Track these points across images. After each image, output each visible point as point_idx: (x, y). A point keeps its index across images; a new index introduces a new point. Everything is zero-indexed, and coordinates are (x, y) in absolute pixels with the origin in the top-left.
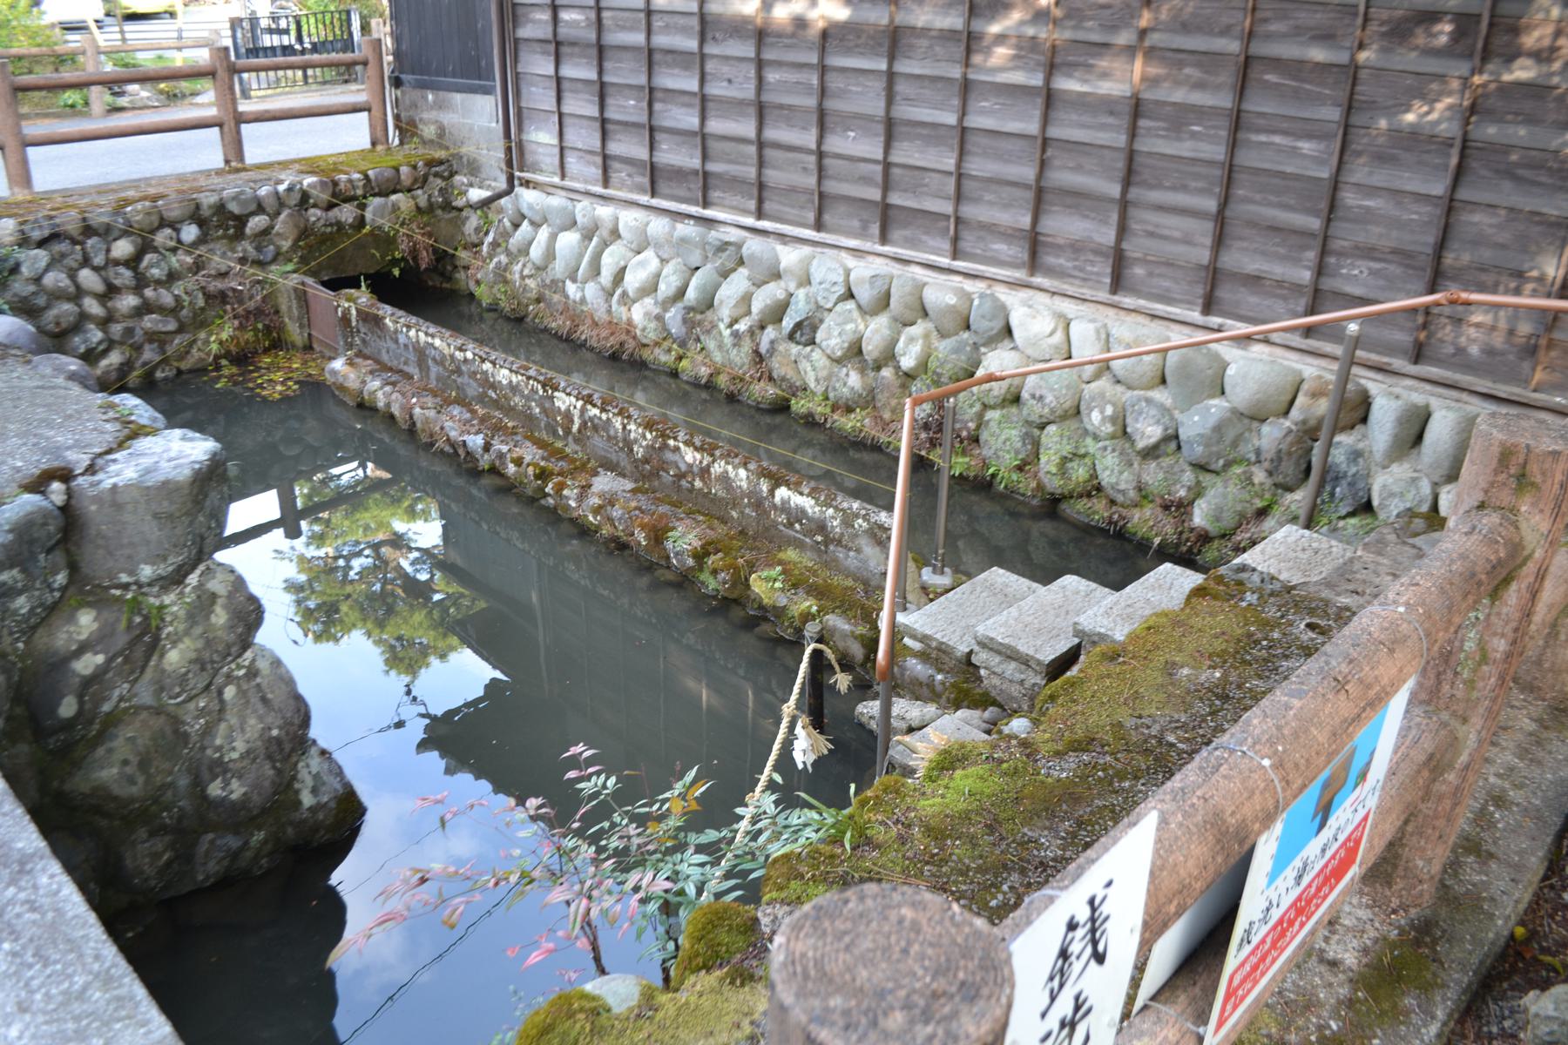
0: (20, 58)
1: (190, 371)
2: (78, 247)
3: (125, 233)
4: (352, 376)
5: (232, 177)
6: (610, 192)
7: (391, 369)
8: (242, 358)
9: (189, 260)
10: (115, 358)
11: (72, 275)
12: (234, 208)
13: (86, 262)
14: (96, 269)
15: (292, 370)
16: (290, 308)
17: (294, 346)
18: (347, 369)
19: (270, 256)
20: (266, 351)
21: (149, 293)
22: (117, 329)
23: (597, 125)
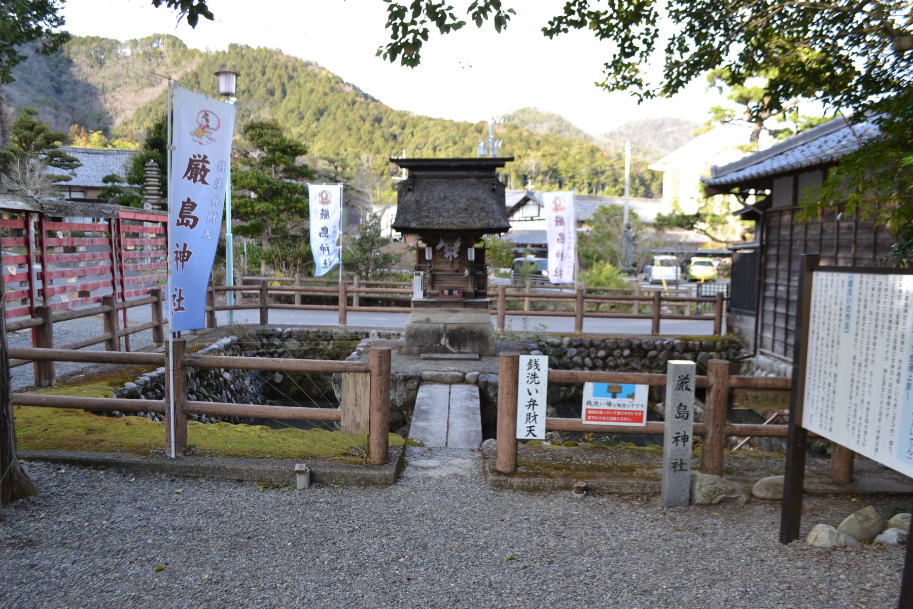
6: (786, 358)
11: (583, 359)
12: (645, 346)
13: (588, 355)
14: (591, 359)
23: (784, 331)
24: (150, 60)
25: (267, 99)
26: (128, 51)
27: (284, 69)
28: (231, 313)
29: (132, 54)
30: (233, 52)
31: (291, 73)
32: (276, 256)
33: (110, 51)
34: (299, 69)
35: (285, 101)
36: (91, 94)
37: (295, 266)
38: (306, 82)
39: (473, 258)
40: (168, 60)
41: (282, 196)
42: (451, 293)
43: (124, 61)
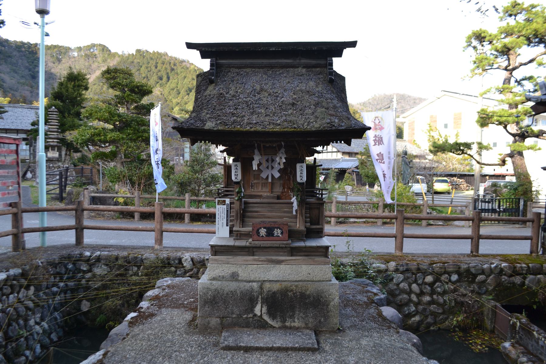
0: (403, 205)
1: (443, 330)
2: (414, 276)
3: (431, 274)
4: (513, 352)
5: (473, 258)
7: (532, 354)
8: (464, 329)
9: (452, 287)
10: (417, 318)
11: (410, 285)
12: (473, 270)
13: (415, 281)
14: (418, 285)
15: (484, 339)
16: (488, 314)
17: (487, 329)
18: (510, 348)
19: (483, 291)
20: (475, 329)
21: (435, 297)
22: (421, 307)
24: (88, 59)
25: (158, 83)
26: (76, 54)
27: (168, 64)
28: (44, 235)
29: (78, 55)
30: (138, 55)
31: (173, 67)
32: (124, 176)
33: (65, 54)
34: (177, 64)
35: (169, 83)
36: (53, 79)
37: (139, 185)
38: (181, 72)
39: (305, 179)
40: (100, 59)
41: (131, 127)
42: (270, 233)
43: (73, 60)
